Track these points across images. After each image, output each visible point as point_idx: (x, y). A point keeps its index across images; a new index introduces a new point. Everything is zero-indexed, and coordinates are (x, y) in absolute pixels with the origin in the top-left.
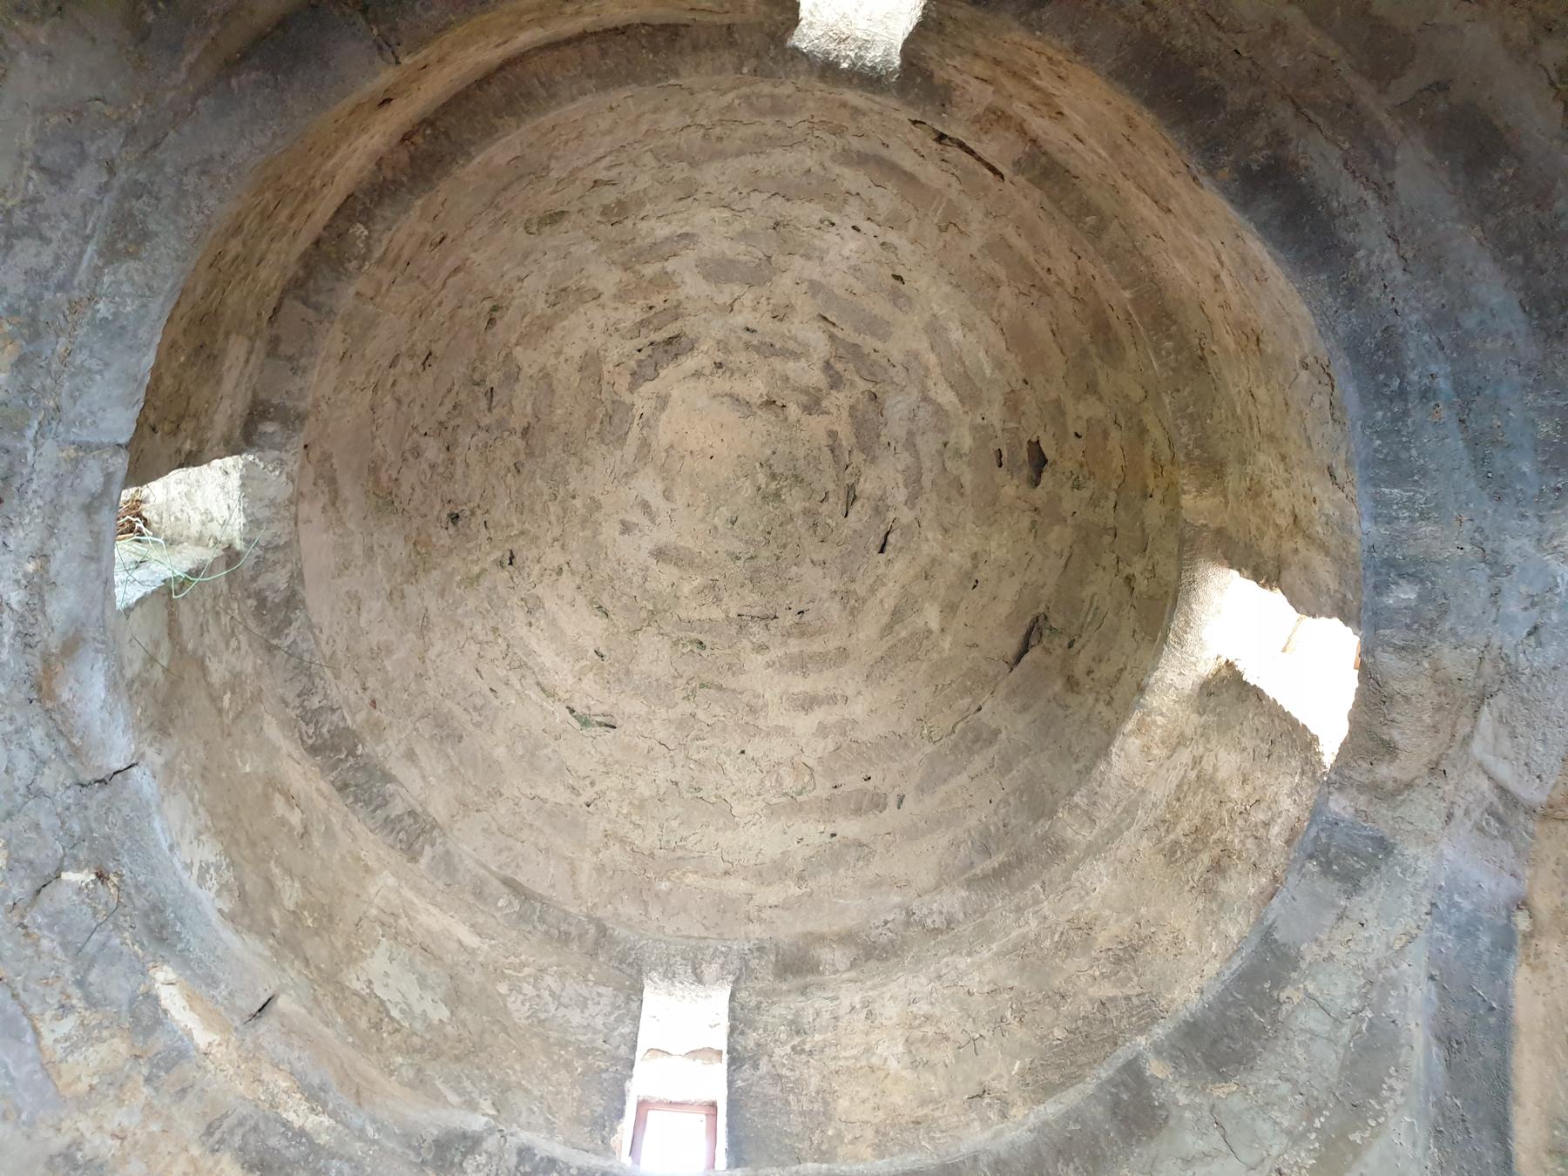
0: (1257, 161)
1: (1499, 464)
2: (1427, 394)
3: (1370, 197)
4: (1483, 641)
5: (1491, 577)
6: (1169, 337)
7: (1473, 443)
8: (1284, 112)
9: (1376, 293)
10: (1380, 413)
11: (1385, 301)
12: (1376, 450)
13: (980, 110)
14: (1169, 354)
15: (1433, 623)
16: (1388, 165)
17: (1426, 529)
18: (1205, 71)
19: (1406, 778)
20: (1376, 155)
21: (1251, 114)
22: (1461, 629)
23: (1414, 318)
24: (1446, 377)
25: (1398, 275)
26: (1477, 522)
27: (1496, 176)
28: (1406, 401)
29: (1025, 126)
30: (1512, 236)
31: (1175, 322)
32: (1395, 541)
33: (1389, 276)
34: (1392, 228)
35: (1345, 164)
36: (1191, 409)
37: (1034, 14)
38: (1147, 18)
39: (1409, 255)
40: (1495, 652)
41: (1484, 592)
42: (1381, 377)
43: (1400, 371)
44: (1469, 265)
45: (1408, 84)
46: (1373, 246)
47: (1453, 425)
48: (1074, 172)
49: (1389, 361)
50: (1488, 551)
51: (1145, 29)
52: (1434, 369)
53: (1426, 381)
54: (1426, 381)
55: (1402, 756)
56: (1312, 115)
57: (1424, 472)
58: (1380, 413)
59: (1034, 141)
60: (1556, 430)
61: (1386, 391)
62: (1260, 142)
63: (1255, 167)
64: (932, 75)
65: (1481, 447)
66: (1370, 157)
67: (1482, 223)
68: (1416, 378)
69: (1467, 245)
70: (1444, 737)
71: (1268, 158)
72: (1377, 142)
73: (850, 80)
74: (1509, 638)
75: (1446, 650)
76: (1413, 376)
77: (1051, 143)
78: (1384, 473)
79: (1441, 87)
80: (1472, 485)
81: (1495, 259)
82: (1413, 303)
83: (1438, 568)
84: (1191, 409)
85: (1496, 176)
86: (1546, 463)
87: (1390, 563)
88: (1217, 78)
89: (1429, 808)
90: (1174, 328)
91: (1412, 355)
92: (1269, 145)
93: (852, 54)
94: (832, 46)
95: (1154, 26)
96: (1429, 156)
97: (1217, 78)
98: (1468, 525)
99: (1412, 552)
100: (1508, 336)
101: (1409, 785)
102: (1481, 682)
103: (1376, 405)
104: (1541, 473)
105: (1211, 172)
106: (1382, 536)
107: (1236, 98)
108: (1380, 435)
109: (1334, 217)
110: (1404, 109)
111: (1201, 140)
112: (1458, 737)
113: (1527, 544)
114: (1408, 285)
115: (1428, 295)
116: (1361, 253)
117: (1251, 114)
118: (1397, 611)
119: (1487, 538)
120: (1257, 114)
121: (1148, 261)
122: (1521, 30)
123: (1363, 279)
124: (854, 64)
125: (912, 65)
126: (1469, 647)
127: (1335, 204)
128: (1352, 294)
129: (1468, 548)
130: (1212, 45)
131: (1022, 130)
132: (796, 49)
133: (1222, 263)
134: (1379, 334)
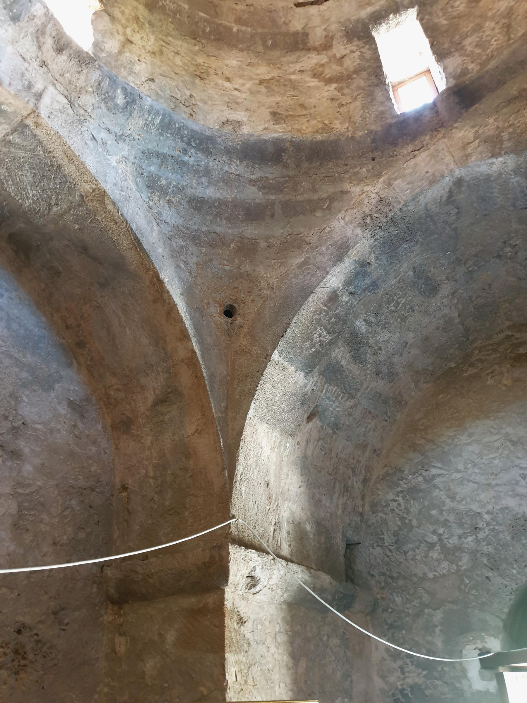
0: (284, 156)
1: (155, 160)
2: (185, 152)
3: (253, 177)
4: (93, 117)
5: (116, 134)
6: (210, 32)
7: (164, 156)
8: (291, 173)
9: (224, 158)
10: (186, 133)
11: (220, 159)
12: (175, 123)
13: (334, 43)
14: (204, 26)
15: (106, 103)
16: (259, 189)
17: (141, 122)
18: (318, 164)
19: (44, 48)
20: (264, 188)
21: (298, 166)
22: (100, 111)
23: (211, 164)
24: (188, 161)
25: (226, 168)
26: (137, 140)
27: (241, 213)
28: (186, 144)
29: (316, 53)
30: (223, 207)
31: (215, 40)
32: (141, 109)
33: (227, 165)
34: (241, 177)
35: (266, 177)
36: (178, 16)
37: (372, 137)
38: (344, 162)
39: (231, 176)
40: (88, 118)
41: (111, 128)
42: (198, 142)
43: (197, 148)
44: (221, 191)
45: (278, 210)
46: (237, 168)
47: (172, 153)
48: (289, 53)
49: (201, 147)
50: (126, 138)
51: (341, 159)
52: (192, 159)
53: (190, 154)
54: (190, 154)
55: (54, 53)
56: (285, 179)
57: (161, 134)
58: (186, 133)
59: (309, 50)
60: (162, 184)
61: (192, 140)
62: (289, 161)
63: (283, 154)
64: (359, 40)
65: (163, 158)
66: (265, 186)
67: (231, 202)
68: (192, 151)
69: (227, 194)
70: (57, 76)
71: (283, 159)
72: (267, 190)
73: (386, 12)
74: (92, 125)
75: (93, 100)
76: (193, 151)
77: (304, 56)
78: (166, 121)
79: (273, 216)
80: (150, 147)
81: (219, 199)
82: (215, 167)
83: (126, 118)
84: (178, 16)
85: (241, 213)
86: (152, 175)
87: (134, 101)
88: (314, 165)
89: (28, 51)
90: (213, 37)
91: (200, 155)
92: (286, 162)
93: (390, 22)
94: (400, 19)
95: (340, 161)
96: (257, 201)
97: (314, 165)
98: (137, 137)
99: (135, 112)
100: (196, 189)
101: (40, 48)
102: (76, 105)
103: (190, 133)
104: (150, 172)
105: (291, 141)
106: (145, 106)
107: (305, 165)
108: (179, 128)
109: (254, 163)
110: (273, 204)
111: (302, 147)
112: (55, 82)
113: (126, 153)
114: (222, 169)
115: (217, 173)
116: (238, 162)
117: (298, 166)
118: (115, 92)
119: (130, 140)
120: (297, 167)
121: (241, 50)
122: (273, 241)
123: (231, 158)
124: (388, 19)
125: (368, 37)
126: (92, 110)
127: (257, 166)
128: (228, 151)
129: (129, 132)
130: (323, 171)
131: (315, 49)
132: (413, 7)
133: (236, 89)
134: (211, 150)
